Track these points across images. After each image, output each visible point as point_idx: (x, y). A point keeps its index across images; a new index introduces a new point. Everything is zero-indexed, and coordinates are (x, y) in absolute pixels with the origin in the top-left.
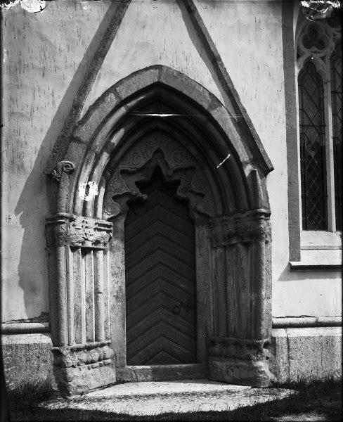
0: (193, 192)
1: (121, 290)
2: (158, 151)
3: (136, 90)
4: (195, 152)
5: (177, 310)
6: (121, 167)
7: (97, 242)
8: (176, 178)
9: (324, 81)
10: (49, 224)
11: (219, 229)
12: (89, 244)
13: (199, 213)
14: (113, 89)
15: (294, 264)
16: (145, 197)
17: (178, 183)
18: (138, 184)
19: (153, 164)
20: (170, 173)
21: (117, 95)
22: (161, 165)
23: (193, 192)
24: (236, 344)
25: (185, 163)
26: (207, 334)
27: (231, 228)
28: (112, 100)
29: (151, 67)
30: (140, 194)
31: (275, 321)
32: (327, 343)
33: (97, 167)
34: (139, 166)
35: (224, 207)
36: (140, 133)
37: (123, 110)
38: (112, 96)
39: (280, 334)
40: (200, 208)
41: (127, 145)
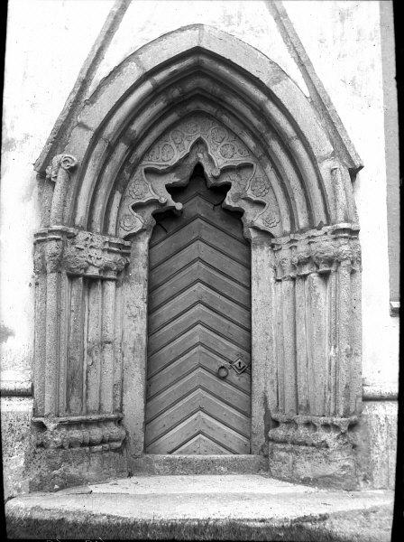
2: (199, 142)
4: (252, 144)
5: (223, 373)
6: (146, 164)
7: (106, 269)
8: (225, 180)
10: (39, 242)
11: (285, 253)
12: (93, 272)
13: (256, 229)
16: (179, 206)
17: (227, 186)
19: (192, 161)
20: (216, 173)
24: (308, 424)
25: (238, 159)
27: (302, 249)
29: (189, 27)
30: (172, 203)
34: (171, 163)
37: (147, 86)
38: (132, 66)
41: (154, 134)
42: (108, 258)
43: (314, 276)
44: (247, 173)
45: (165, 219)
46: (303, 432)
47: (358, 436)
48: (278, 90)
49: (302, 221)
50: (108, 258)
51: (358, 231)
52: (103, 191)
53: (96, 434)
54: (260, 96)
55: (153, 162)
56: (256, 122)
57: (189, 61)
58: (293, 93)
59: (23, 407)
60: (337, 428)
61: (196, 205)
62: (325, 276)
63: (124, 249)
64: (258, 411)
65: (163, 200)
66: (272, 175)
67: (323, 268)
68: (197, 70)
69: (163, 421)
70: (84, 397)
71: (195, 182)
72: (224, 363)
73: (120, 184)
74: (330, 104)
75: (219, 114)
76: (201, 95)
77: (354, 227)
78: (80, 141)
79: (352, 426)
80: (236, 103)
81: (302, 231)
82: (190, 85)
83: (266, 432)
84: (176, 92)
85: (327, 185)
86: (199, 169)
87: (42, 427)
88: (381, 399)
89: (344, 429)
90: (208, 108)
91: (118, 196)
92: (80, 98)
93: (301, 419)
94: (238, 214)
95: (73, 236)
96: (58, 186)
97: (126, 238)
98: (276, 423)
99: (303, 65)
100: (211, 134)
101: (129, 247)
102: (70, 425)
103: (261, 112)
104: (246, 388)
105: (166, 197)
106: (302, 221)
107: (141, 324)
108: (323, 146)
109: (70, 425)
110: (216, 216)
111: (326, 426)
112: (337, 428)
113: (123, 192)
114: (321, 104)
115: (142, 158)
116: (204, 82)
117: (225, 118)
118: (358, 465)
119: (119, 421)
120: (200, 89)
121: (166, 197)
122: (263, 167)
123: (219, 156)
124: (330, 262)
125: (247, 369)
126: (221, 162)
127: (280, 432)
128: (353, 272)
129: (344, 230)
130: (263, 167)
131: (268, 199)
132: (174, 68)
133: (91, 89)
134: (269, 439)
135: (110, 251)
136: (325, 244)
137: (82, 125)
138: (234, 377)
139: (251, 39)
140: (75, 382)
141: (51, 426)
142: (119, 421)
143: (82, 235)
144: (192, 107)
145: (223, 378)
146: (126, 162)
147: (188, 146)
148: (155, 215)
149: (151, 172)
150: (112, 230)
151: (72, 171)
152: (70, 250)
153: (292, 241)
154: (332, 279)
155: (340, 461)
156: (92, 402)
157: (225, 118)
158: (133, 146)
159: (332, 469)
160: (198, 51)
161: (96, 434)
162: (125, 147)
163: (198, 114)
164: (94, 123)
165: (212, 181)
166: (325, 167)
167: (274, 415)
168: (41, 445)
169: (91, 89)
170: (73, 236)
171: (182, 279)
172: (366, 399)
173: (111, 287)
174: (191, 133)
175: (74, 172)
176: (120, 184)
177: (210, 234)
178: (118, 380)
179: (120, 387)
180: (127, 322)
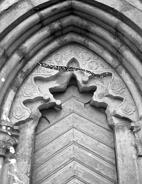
0: (109, 96)
2: (74, 61)
6: (35, 74)
8: (91, 84)
16: (58, 102)
23: (109, 96)
37: (35, 17)
44: (107, 80)
61: (71, 103)
75: (86, 42)
82: (66, 21)
86: (73, 81)
97: (17, 124)
131: (125, 95)
144: (68, 38)
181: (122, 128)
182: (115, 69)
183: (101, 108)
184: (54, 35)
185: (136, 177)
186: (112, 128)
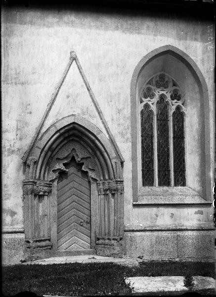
0: (90, 169)
1: (56, 215)
2: (74, 149)
3: (150, 203)
4: (91, 151)
5: (82, 224)
6: (56, 157)
7: (45, 192)
8: (81, 162)
9: (169, 116)
10: (25, 185)
11: (101, 186)
12: (41, 193)
13: (92, 178)
14: (53, 125)
15: (134, 203)
16: (67, 170)
17: (83, 164)
18: (64, 164)
19: (71, 155)
20: (79, 159)
21: (56, 128)
22: (75, 155)
23: (90, 169)
24: (108, 239)
25: (87, 155)
26: (96, 236)
27: (107, 187)
28: (53, 130)
29: (71, 115)
30: (65, 169)
31: (126, 229)
32: (46, 97)
33: (148, 65)
34: (65, 156)
35: (104, 176)
36: (65, 142)
37: (58, 134)
38: (53, 128)
39: (129, 234)
40: (93, 176)
41: (59, 147)
42: (46, 188)
43: (110, 194)
44: (89, 160)
45: (62, 175)
46: (107, 241)
47: (122, 242)
48: (98, 136)
49: (107, 177)
50: (46, 188)
51: (123, 181)
52: (43, 168)
53: (43, 244)
54: (93, 138)
55: (61, 157)
56: (92, 145)
57: (71, 126)
58: (104, 137)
59: (22, 236)
60: (116, 240)
61: (72, 170)
62: (113, 195)
63: (50, 186)
64: (93, 235)
65: (62, 169)
66: (97, 161)
67: (114, 192)
68: (74, 128)
69: (62, 240)
70: (39, 233)
71: (72, 162)
72: (83, 221)
73: (48, 164)
74: (115, 142)
75: (80, 141)
76: (74, 135)
77: (122, 180)
78: (37, 152)
79: (121, 239)
80: (86, 139)
81: (106, 180)
82: (71, 133)
83: (96, 242)
84: (66, 135)
85: (114, 167)
86: (73, 158)
87: (28, 242)
88: (39, 148)
89: (119, 240)
90: (76, 139)
91: (48, 168)
92: (36, 139)
93: (107, 237)
94: (87, 172)
95: (36, 183)
96: (31, 167)
97: (50, 181)
98: (99, 239)
99: (107, 129)
100: (77, 147)
101: (51, 184)
102: (37, 241)
103: (93, 142)
104: (89, 229)
105: (63, 168)
106: (107, 177)
107: (56, 209)
108: (113, 154)
109: (37, 241)
110: (80, 174)
111: (114, 239)
112: (116, 240)
113: (49, 166)
114: (112, 141)
115: (55, 155)
116: (76, 132)
117: (82, 142)
118: (123, 250)
119: (49, 240)
120: (75, 135)
121: (63, 168)
122: (94, 158)
123: (80, 155)
124: (115, 190)
125: (90, 223)
126: (81, 156)
127: (101, 241)
128: (121, 194)
129: (119, 181)
130: (94, 158)
131: (96, 168)
132: (66, 128)
133: (40, 136)
134: (97, 244)
135: (46, 186)
136: (113, 185)
137: (37, 147)
138: (85, 225)
139: (92, 122)
140: (37, 227)
141: (31, 241)
142: (49, 240)
143: (38, 182)
144: (71, 139)
145: (82, 226)
146: (50, 156)
147: (70, 151)
148: (59, 173)
149: (58, 159)
150: (46, 179)
151: (35, 162)
152: (35, 187)
153: (104, 183)
154: (116, 195)
155: (117, 249)
156: (42, 234)
157: (82, 142)
158: (53, 152)
159: (115, 252)
160: (74, 123)
161: (43, 244)
162: (51, 154)
163: (73, 140)
164: (42, 147)
165: (78, 162)
166: (113, 161)
167: (98, 237)
168: (29, 248)
169: (40, 136)
170: (36, 183)
171: (68, 194)
172: (125, 231)
173: (46, 198)
174: (71, 146)
175: (36, 163)
176: (48, 164)
177: (77, 179)
178: (49, 228)
179: (50, 229)
180: (51, 209)
181: (94, 183)
182: (93, 156)
183: (85, 174)
184: (69, 142)
185: (77, 268)
186: (89, 182)
